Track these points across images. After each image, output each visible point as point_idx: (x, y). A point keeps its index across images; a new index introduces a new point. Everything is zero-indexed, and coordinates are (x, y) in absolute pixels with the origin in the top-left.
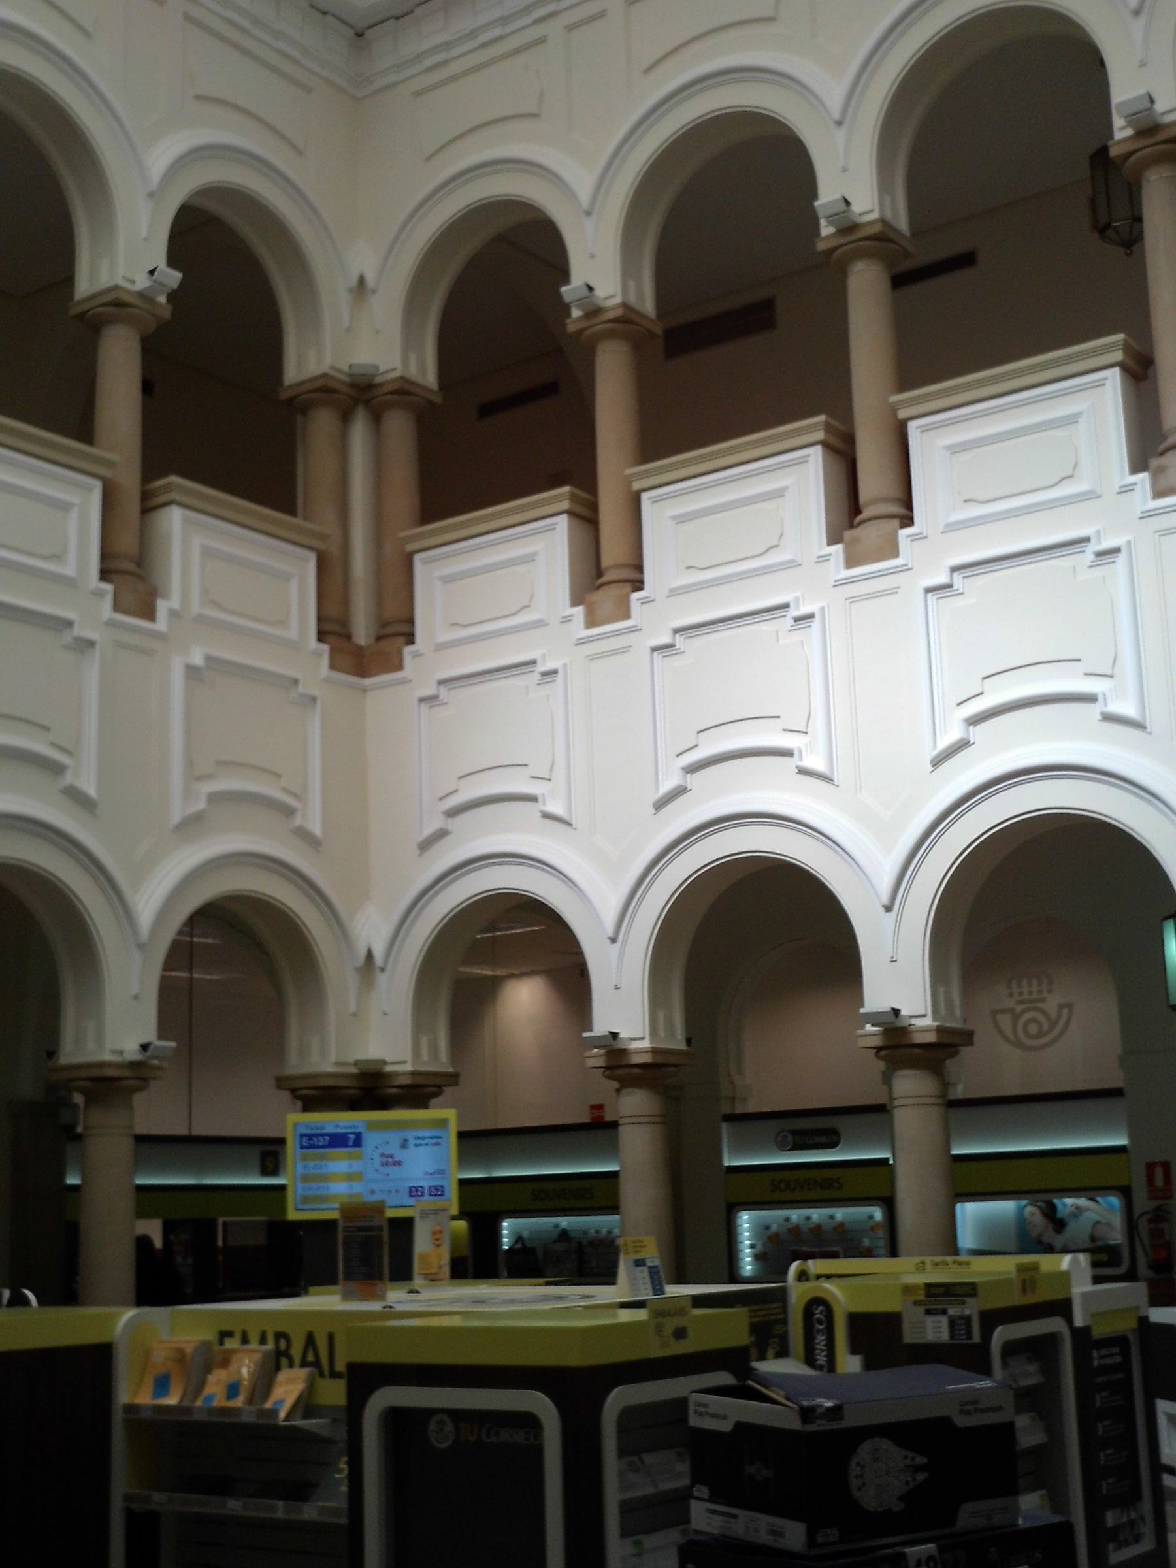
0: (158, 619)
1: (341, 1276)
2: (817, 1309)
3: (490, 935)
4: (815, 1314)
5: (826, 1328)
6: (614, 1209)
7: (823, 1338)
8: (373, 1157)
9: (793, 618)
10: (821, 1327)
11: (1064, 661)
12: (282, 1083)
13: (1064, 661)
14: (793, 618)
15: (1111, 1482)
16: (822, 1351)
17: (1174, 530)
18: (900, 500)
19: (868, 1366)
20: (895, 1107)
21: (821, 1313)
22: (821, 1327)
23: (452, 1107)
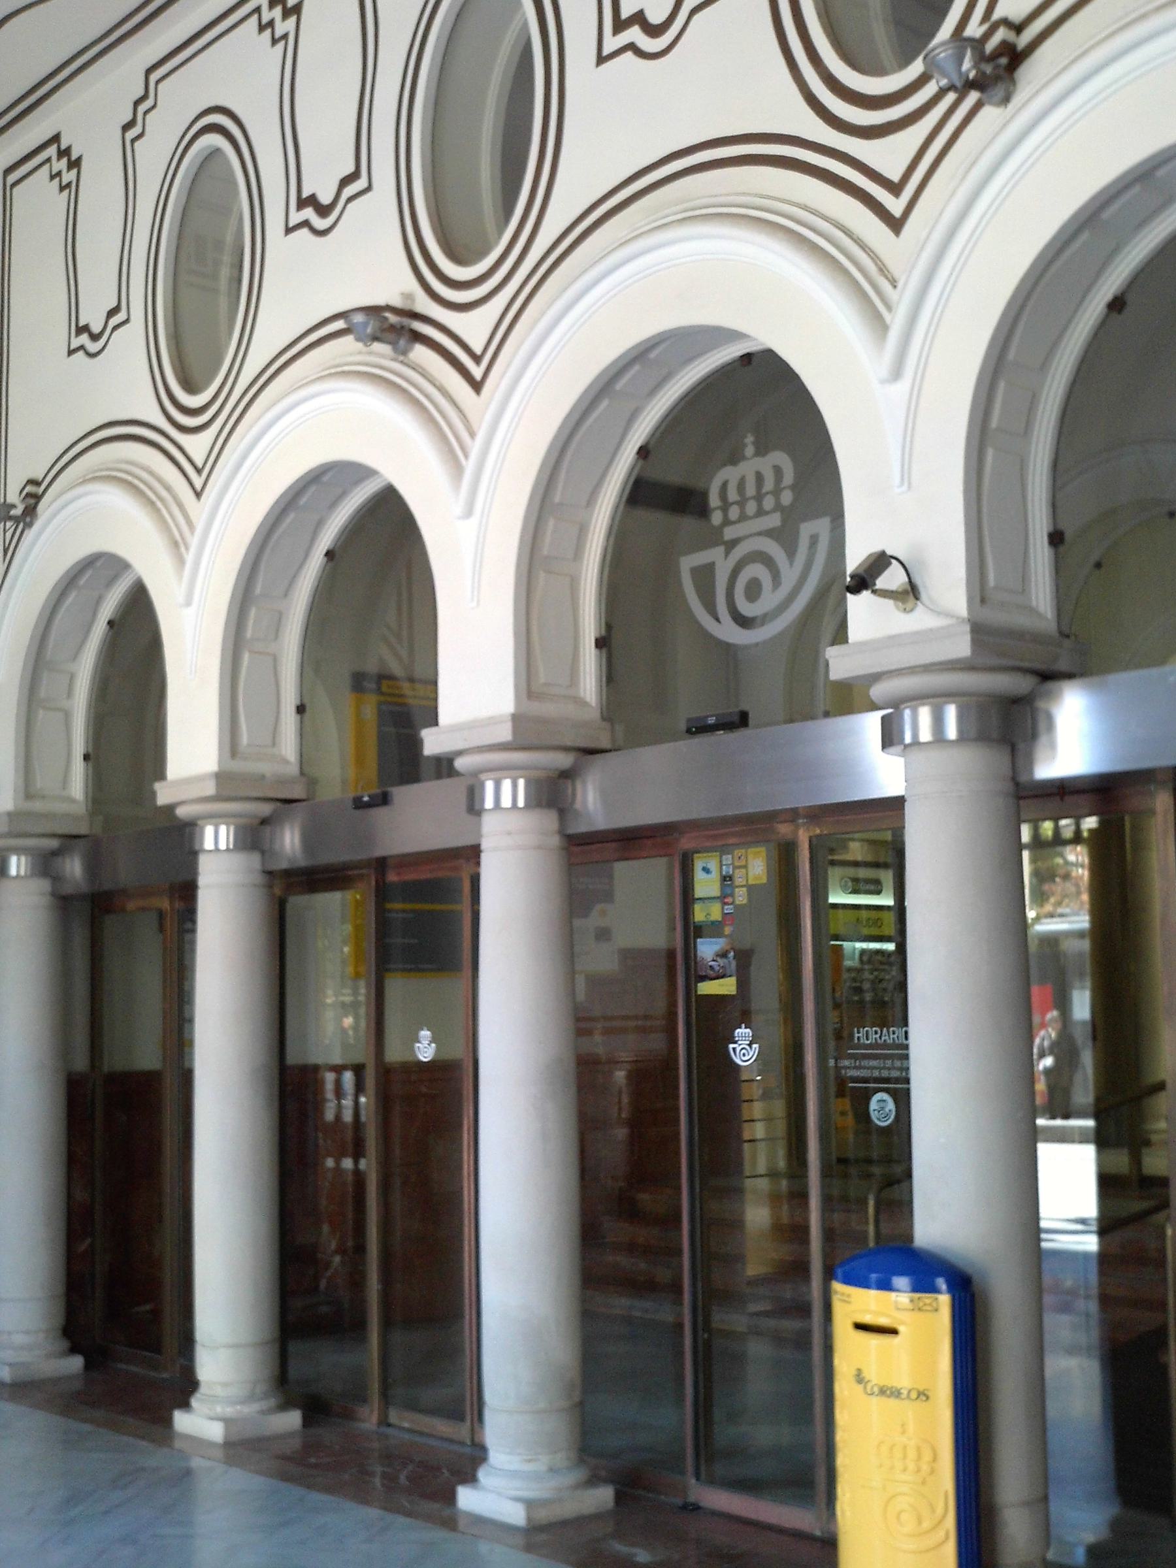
1: (906, 1052)
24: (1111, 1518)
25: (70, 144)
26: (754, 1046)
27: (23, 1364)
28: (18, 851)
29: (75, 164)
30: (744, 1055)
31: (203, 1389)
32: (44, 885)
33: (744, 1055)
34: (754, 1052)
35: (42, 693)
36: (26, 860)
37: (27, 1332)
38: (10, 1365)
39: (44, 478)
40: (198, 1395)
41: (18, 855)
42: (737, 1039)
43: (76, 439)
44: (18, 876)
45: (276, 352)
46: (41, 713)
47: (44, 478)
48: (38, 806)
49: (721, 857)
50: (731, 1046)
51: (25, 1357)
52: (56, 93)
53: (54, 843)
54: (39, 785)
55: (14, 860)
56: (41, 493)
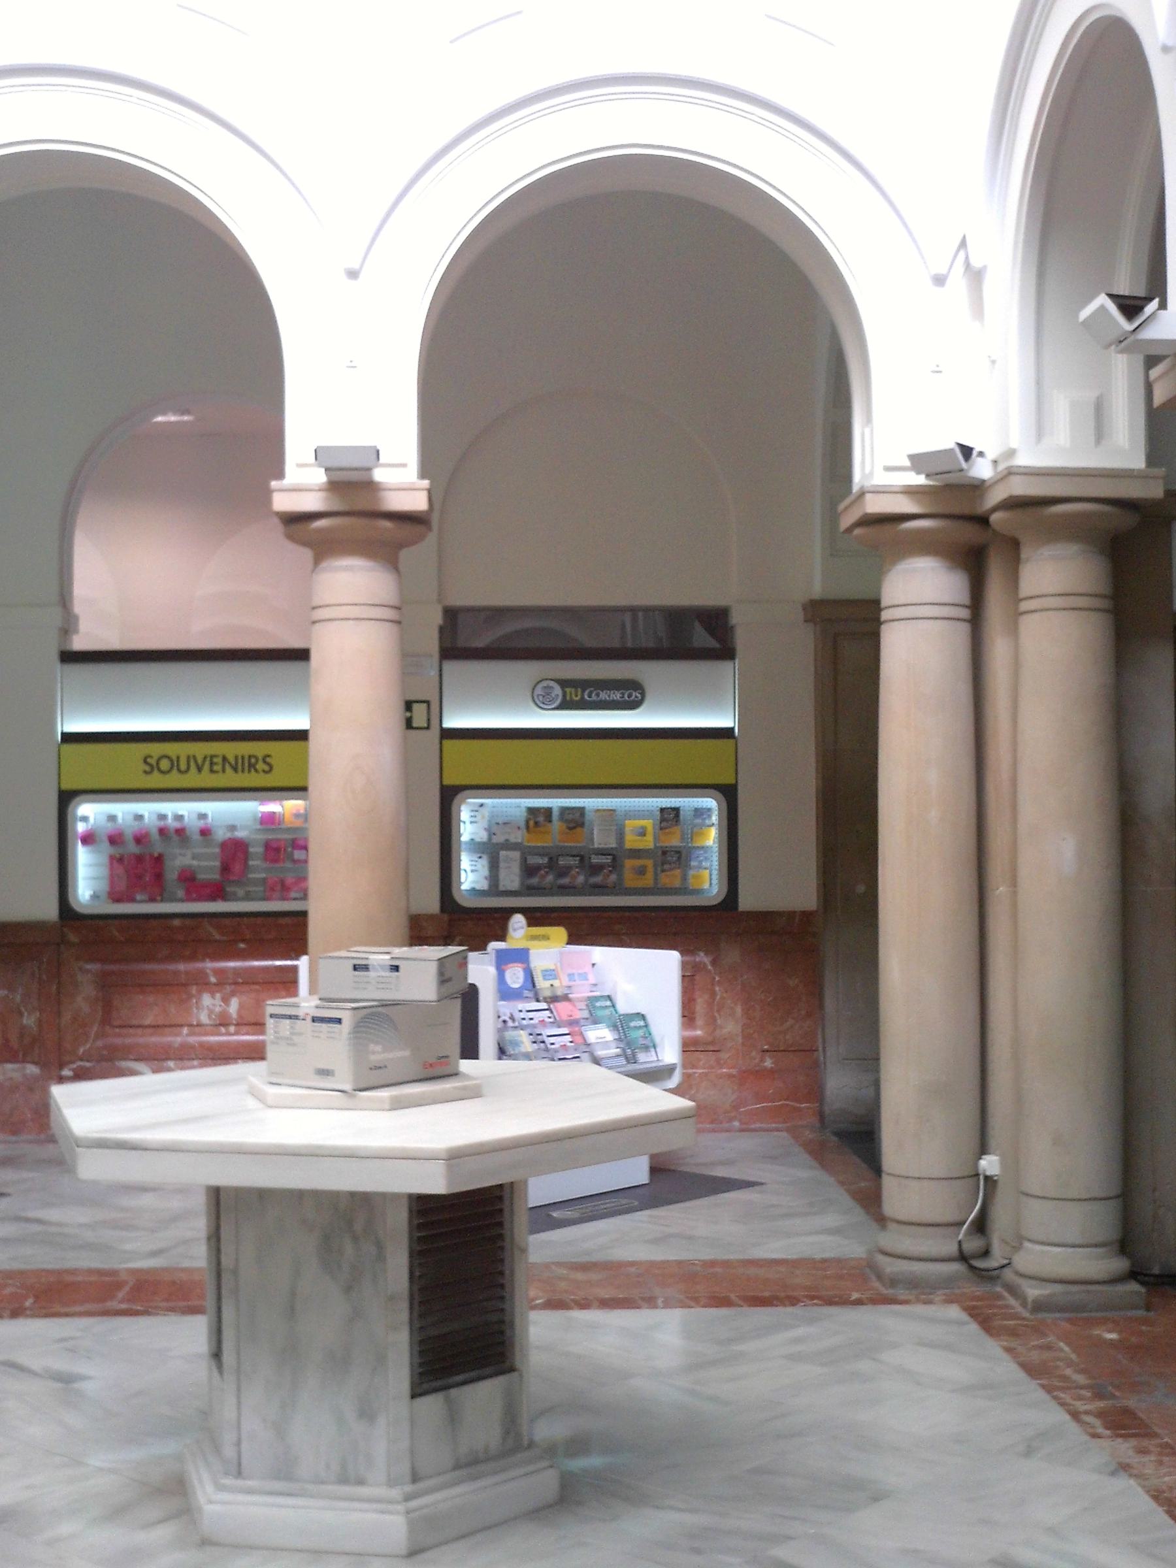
0: (907, 457)
2: (639, 693)
3: (487, 1209)
4: (635, 691)
5: (626, 700)
6: (300, 790)
7: (618, 697)
8: (1065, 842)
9: (985, 267)
10: (626, 696)
11: (198, 188)
12: (1169, 356)
13: (198, 188)
14: (985, 267)
15: (481, 1298)
16: (609, 696)
18: (385, 490)
19: (306, 953)
20: (1021, 600)
21: (636, 697)
22: (626, 696)
23: (743, 912)
49: (967, 607)
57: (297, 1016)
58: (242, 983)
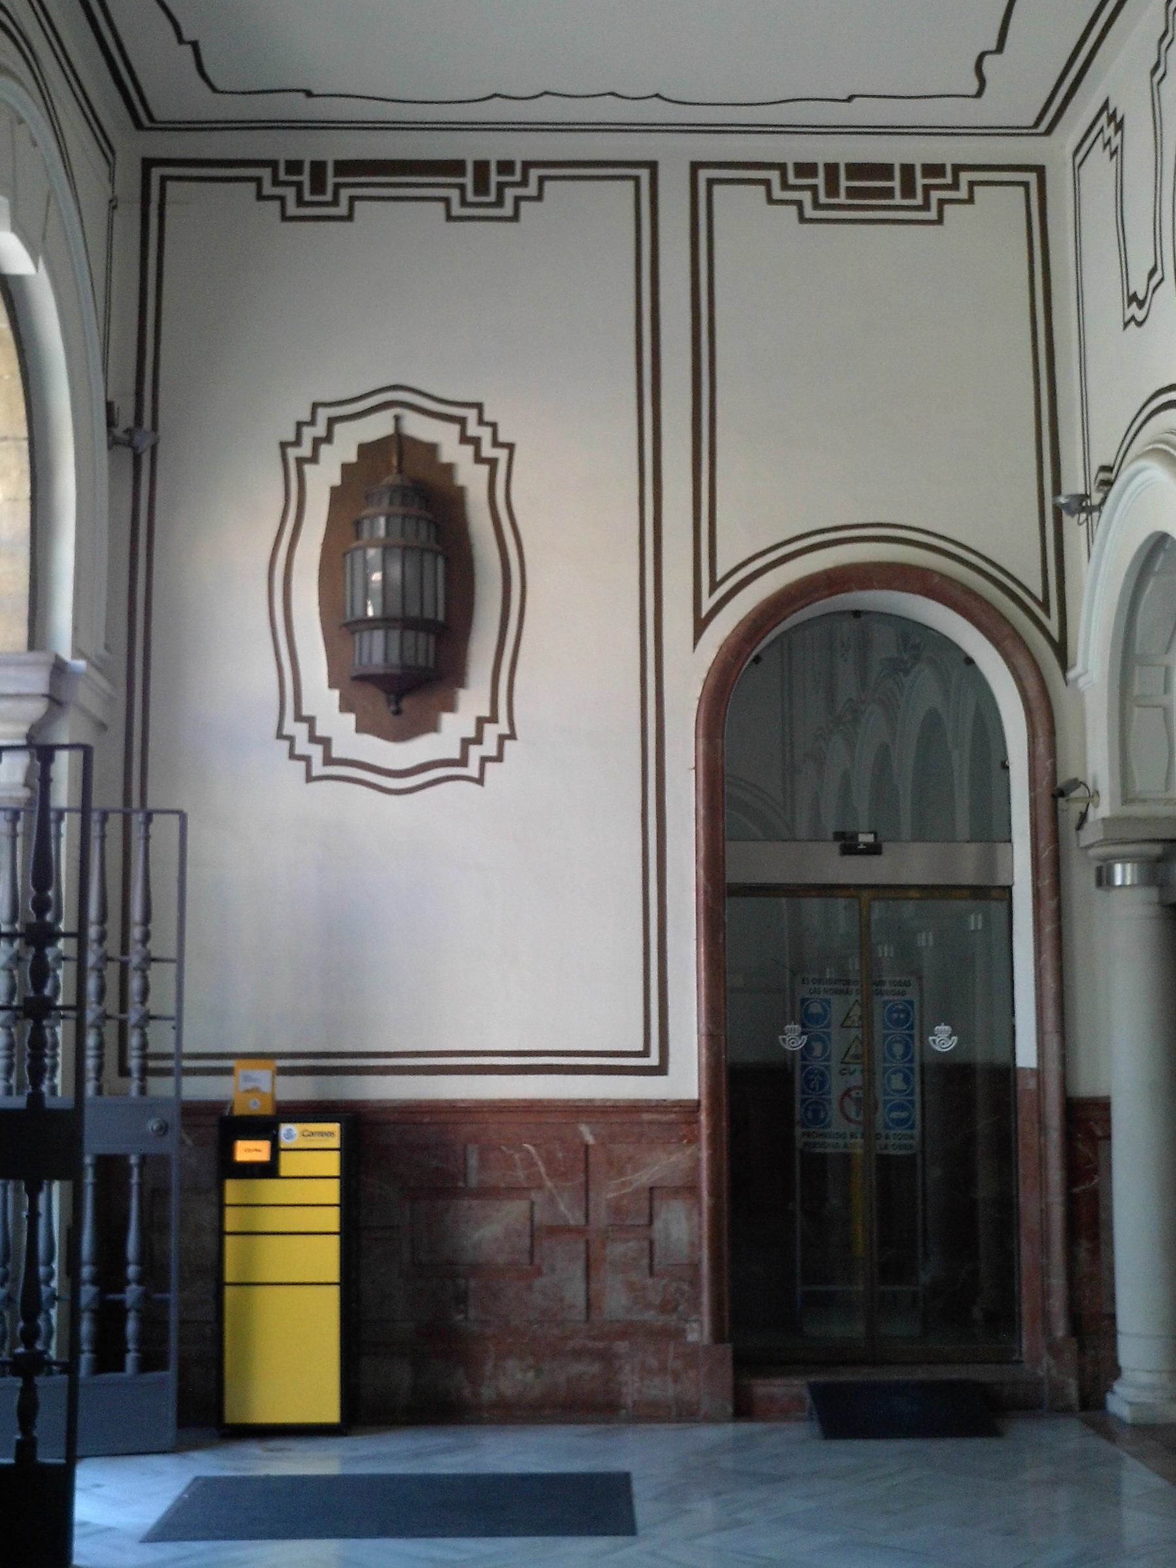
17: (36, 4)
24: (1065, 1290)
25: (1115, 106)
26: (953, 1038)
27: (1142, 1404)
28: (1123, 859)
29: (1120, 127)
30: (793, 1043)
31: (1126, 1374)
32: (1152, 894)
33: (793, 1043)
34: (802, 1043)
35: (1136, 690)
36: (1132, 867)
37: (1160, 1372)
38: (1130, 1404)
39: (1115, 462)
40: (1120, 1381)
41: (1124, 863)
42: (936, 1033)
43: (908, 524)
44: (1122, 886)
45: (1135, 413)
46: (1136, 711)
47: (1115, 462)
48: (1137, 810)
50: (931, 1038)
51: (1146, 1397)
52: (92, 776)
53: (1157, 849)
54: (1138, 787)
55: (1118, 868)
56: (1113, 478)
57: (757, 663)
58: (861, 931)
